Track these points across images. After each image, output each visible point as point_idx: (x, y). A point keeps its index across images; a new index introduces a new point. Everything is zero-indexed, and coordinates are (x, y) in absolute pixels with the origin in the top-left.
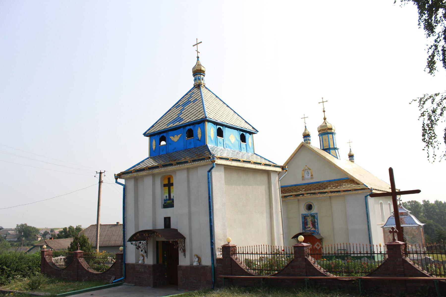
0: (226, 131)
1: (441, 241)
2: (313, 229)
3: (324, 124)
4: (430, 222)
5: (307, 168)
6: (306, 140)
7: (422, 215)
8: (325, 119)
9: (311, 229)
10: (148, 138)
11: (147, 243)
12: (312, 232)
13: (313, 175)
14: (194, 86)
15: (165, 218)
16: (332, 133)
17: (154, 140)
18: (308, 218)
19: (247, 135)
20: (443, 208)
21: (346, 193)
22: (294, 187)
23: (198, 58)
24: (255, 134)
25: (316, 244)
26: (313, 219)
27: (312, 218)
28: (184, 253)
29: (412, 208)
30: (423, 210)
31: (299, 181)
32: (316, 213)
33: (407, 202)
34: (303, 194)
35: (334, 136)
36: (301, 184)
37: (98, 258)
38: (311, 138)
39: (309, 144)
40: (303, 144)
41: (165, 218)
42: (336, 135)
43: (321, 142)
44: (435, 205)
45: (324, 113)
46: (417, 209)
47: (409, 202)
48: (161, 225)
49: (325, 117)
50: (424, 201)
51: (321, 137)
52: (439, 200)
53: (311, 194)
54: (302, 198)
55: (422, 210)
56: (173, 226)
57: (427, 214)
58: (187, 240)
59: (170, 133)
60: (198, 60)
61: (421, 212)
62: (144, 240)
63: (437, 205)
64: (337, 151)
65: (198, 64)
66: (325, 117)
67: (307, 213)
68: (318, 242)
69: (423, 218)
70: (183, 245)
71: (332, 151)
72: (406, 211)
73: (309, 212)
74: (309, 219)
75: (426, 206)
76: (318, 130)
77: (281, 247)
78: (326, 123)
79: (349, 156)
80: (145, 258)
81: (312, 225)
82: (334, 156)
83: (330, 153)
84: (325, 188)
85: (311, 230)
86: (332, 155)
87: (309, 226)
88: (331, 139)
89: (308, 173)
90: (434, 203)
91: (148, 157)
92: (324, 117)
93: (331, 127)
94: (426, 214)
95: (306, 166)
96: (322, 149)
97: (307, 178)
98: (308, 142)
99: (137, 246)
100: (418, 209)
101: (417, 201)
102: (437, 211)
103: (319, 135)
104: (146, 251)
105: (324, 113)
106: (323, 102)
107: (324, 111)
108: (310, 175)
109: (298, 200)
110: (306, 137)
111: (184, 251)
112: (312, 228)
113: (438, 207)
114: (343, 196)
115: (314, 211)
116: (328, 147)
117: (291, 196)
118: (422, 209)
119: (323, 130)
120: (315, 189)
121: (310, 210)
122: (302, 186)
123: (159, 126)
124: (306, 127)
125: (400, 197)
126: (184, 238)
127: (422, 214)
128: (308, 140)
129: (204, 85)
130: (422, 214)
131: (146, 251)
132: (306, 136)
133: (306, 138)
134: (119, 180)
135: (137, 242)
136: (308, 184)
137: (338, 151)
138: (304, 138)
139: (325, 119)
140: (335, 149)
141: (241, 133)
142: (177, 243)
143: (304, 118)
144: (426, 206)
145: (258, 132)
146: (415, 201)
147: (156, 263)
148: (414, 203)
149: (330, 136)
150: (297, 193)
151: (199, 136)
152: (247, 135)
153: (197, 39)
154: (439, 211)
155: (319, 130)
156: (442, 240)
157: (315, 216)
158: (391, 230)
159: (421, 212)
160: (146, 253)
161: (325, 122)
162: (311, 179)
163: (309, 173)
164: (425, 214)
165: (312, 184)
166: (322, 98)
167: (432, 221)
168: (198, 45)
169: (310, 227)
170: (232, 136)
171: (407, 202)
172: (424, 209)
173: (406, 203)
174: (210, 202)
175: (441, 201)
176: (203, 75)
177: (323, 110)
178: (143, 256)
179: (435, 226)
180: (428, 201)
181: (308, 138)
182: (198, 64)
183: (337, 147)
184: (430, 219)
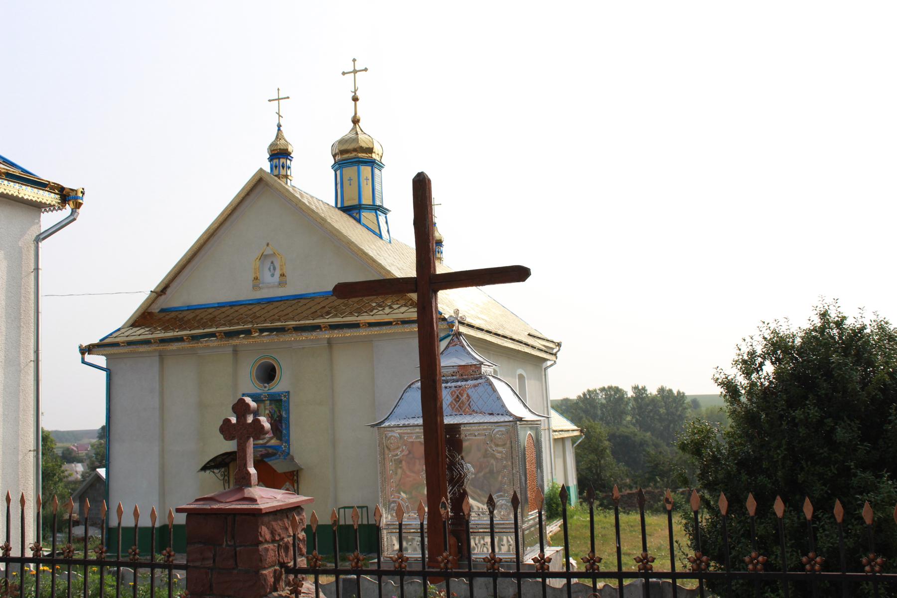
1: (657, 480)
2: (274, 442)
3: (353, 135)
4: (644, 436)
6: (276, 167)
7: (629, 421)
8: (356, 121)
12: (270, 451)
16: (372, 163)
20: (674, 405)
21: (375, 330)
22: (229, 308)
26: (276, 410)
27: (273, 406)
29: (609, 403)
30: (633, 409)
31: (245, 293)
32: (286, 392)
33: (599, 390)
34: (248, 332)
35: (377, 171)
36: (247, 302)
39: (285, 180)
40: (264, 175)
42: (383, 170)
43: (339, 186)
44: (658, 398)
46: (620, 405)
47: (603, 389)
49: (356, 114)
50: (636, 388)
51: (338, 172)
52: (668, 387)
53: (271, 330)
54: (245, 342)
55: (629, 408)
57: (641, 419)
61: (627, 414)
63: (663, 400)
64: (382, 218)
66: (356, 114)
67: (259, 391)
69: (632, 426)
71: (367, 216)
72: (475, 359)
73: (265, 387)
74: (265, 409)
75: (640, 400)
76: (332, 150)
77: (23, 501)
78: (357, 134)
82: (374, 233)
83: (359, 221)
85: (268, 445)
86: (364, 225)
88: (367, 179)
89: (272, 267)
90: (657, 393)
92: (353, 114)
93: (371, 147)
94: (638, 417)
96: (339, 209)
97: (268, 283)
98: (283, 172)
100: (622, 406)
101: (620, 387)
102: (662, 411)
103: (333, 167)
106: (355, 72)
107: (355, 99)
108: (277, 273)
109: (235, 351)
110: (276, 158)
112: (271, 438)
113: (665, 403)
114: (368, 340)
115: (279, 386)
116: (356, 202)
117: (212, 335)
118: (631, 407)
119: (342, 152)
121: (268, 384)
122: (250, 307)
124: (281, 128)
125: (555, 362)
127: (629, 418)
130: (629, 418)
133: (275, 161)
134: (88, 358)
136: (270, 301)
137: (386, 217)
138: (270, 161)
139: (356, 121)
140: (378, 209)
143: (278, 99)
144: (640, 400)
146: (615, 387)
147: (264, 512)
148: (613, 393)
149: (366, 170)
150: (232, 328)
153: (278, 89)
154: (665, 411)
156: (657, 477)
157: (281, 400)
158: (234, 420)
159: (628, 414)
161: (354, 129)
162: (278, 287)
163: (274, 269)
164: (636, 418)
165: (281, 301)
166: (354, 60)
167: (649, 434)
168: (280, 101)
171: (599, 390)
172: (635, 406)
173: (595, 391)
174: (110, 380)
175: (671, 388)
177: (354, 94)
179: (654, 445)
180: (645, 387)
181: (282, 161)
183: (385, 206)
184: (646, 431)
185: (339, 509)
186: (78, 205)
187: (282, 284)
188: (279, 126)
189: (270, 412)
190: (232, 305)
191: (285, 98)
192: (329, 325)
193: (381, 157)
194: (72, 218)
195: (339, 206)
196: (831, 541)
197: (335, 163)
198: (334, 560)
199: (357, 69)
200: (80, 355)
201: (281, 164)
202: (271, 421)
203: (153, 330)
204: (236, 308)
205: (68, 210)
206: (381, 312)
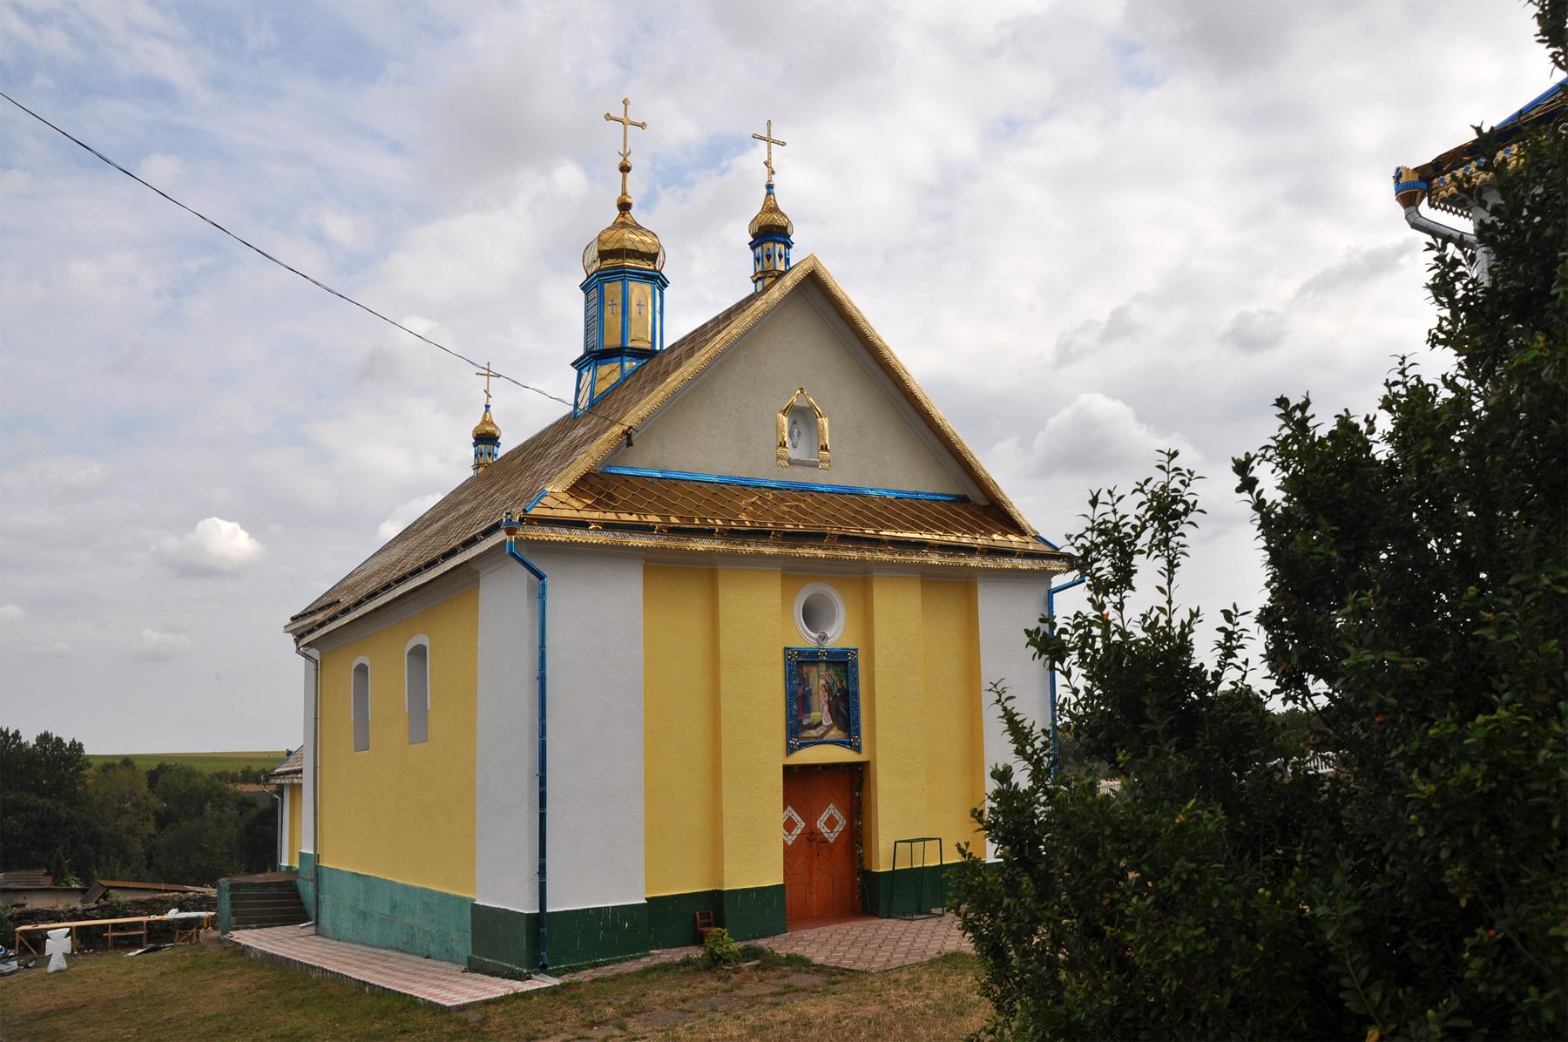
9: (824, 735)
18: (814, 670)
23: (487, 407)
25: (825, 816)
26: (836, 678)
27: (831, 672)
32: (854, 650)
45: (624, 179)
65: (771, 208)
66: (624, 194)
68: (831, 806)
81: (830, 711)
87: (815, 716)
105: (624, 179)
107: (625, 169)
112: (830, 728)
124: (775, 190)
133: (482, 447)
169: (820, 723)
182: (485, 422)
185: (896, 843)
188: (770, 187)
189: (827, 682)
196: (1375, 756)
202: (829, 697)
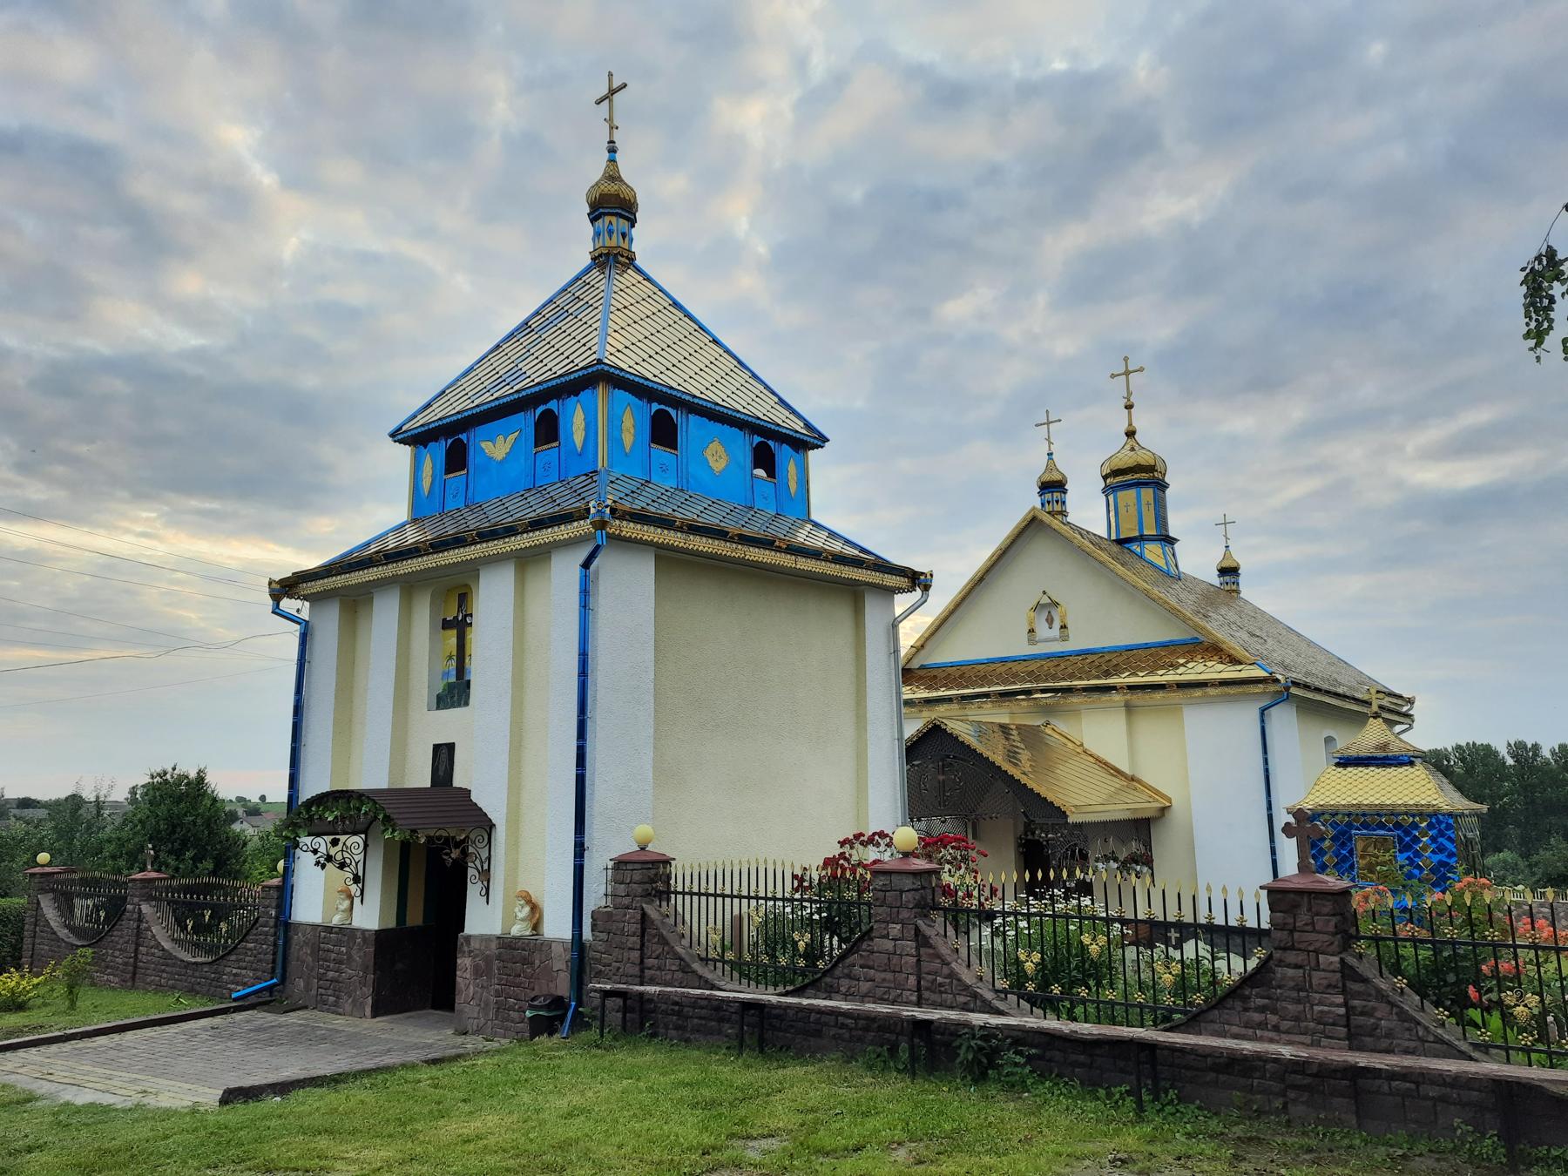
0: (690, 428)
5: (1045, 600)
6: (1049, 502)
10: (406, 451)
11: (366, 846)
13: (1068, 626)
14: (594, 259)
15: (437, 748)
17: (428, 455)
19: (783, 453)
24: (820, 449)
28: (485, 883)
37: (775, 899)
38: (1072, 498)
41: (437, 748)
43: (1112, 514)
45: (1130, 414)
48: (420, 777)
50: (1520, 745)
51: (1111, 498)
56: (459, 781)
58: (500, 835)
59: (481, 430)
60: (612, 161)
62: (355, 833)
65: (613, 176)
70: (484, 855)
79: (1219, 571)
80: (357, 901)
84: (1107, 674)
91: (405, 519)
95: (1044, 593)
99: (319, 854)
104: (360, 874)
105: (1130, 414)
107: (1129, 407)
108: (1057, 625)
111: (486, 875)
119: (1116, 473)
120: (1072, 676)
123: (449, 403)
126: (490, 827)
128: (1057, 502)
129: (627, 258)
131: (360, 874)
132: (1053, 487)
133: (1048, 496)
134: (288, 604)
135: (319, 839)
141: (757, 439)
142: (462, 845)
145: (828, 440)
147: (392, 924)
151: (578, 438)
152: (783, 453)
155: (1104, 474)
160: (360, 885)
170: (715, 447)
176: (627, 219)
178: (351, 897)
183: (1171, 534)
186: (926, 588)
187: (1064, 638)
190: (1003, 661)
191: (1056, 421)
192: (1127, 686)
193: (1165, 474)
194: (923, 599)
195: (1113, 537)
197: (1106, 486)
198: (1241, 950)
199: (1130, 369)
200: (270, 602)
201: (1055, 499)
203: (915, 689)
204: (1009, 665)
205: (918, 592)
206: (1171, 672)
